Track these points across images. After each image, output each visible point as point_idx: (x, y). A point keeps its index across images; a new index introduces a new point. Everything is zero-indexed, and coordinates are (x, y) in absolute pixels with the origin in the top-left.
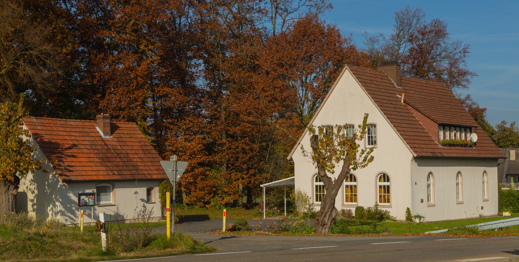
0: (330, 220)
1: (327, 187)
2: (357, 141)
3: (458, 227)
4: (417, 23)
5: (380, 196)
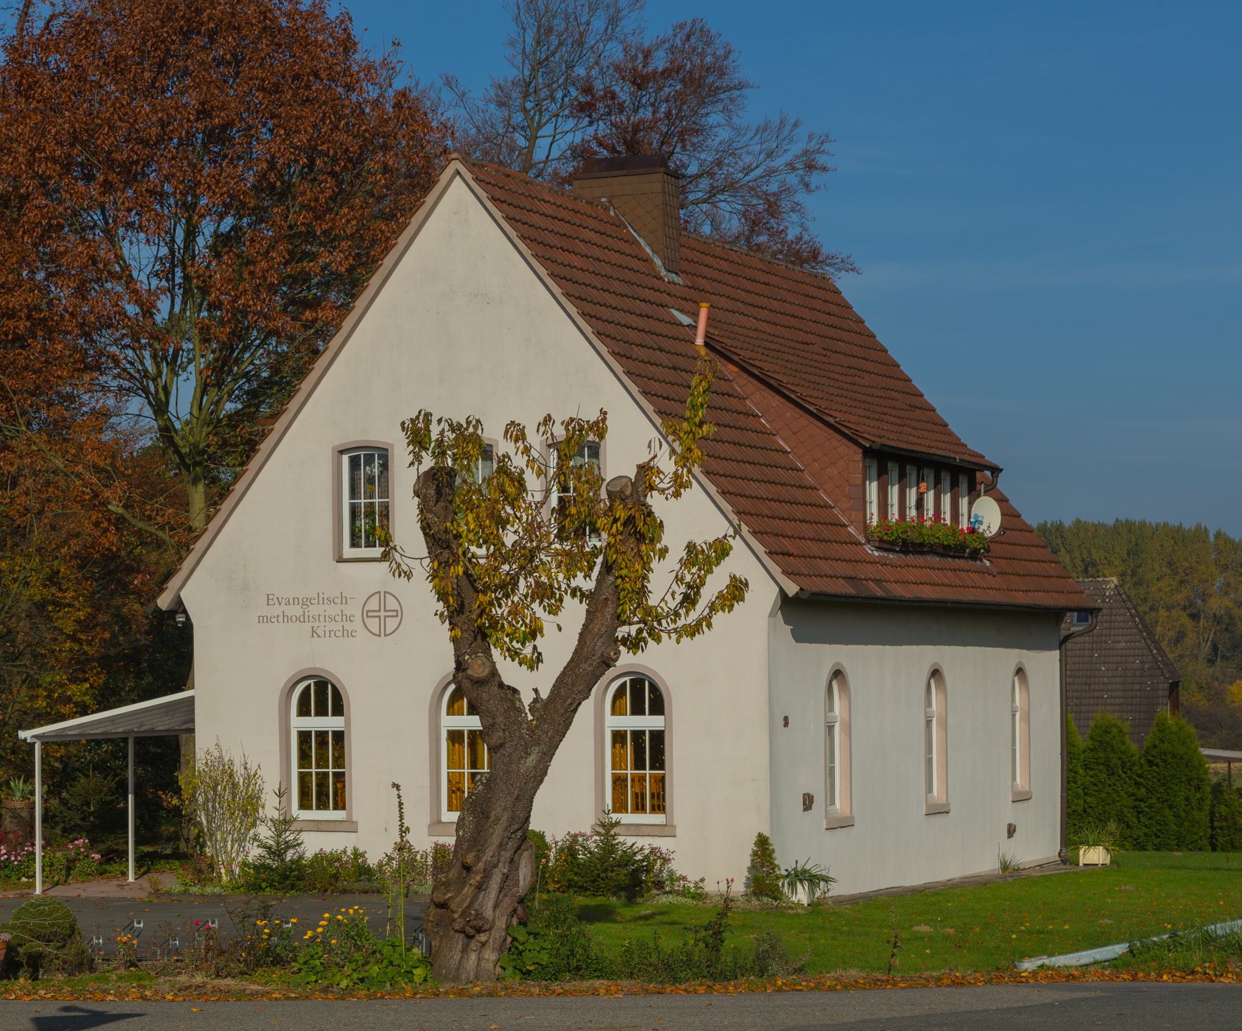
0: (508, 903)
1: (497, 737)
2: (655, 501)
3: (1174, 935)
4: (608, 35)
5: (619, 782)
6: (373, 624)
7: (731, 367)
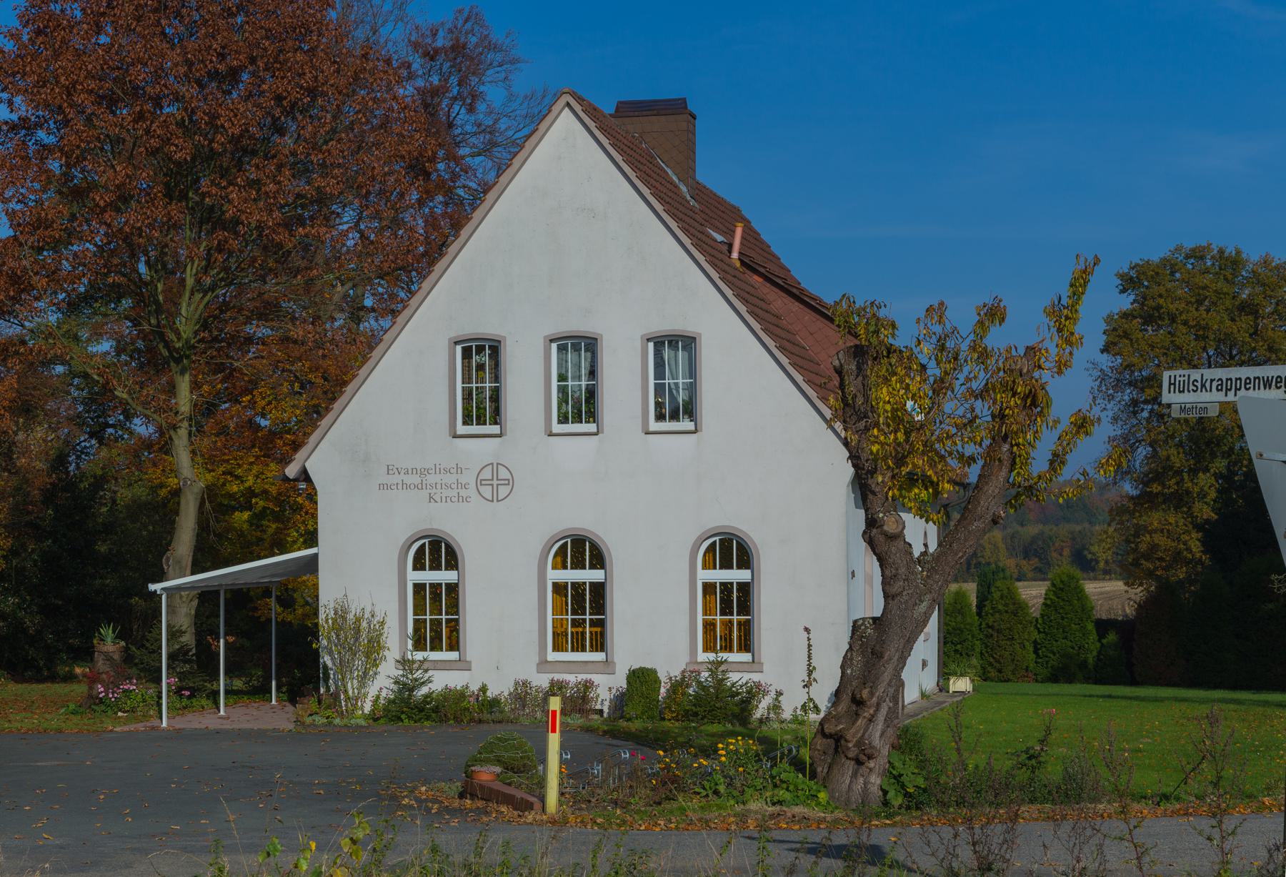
6: (487, 491)
7: (756, 277)
